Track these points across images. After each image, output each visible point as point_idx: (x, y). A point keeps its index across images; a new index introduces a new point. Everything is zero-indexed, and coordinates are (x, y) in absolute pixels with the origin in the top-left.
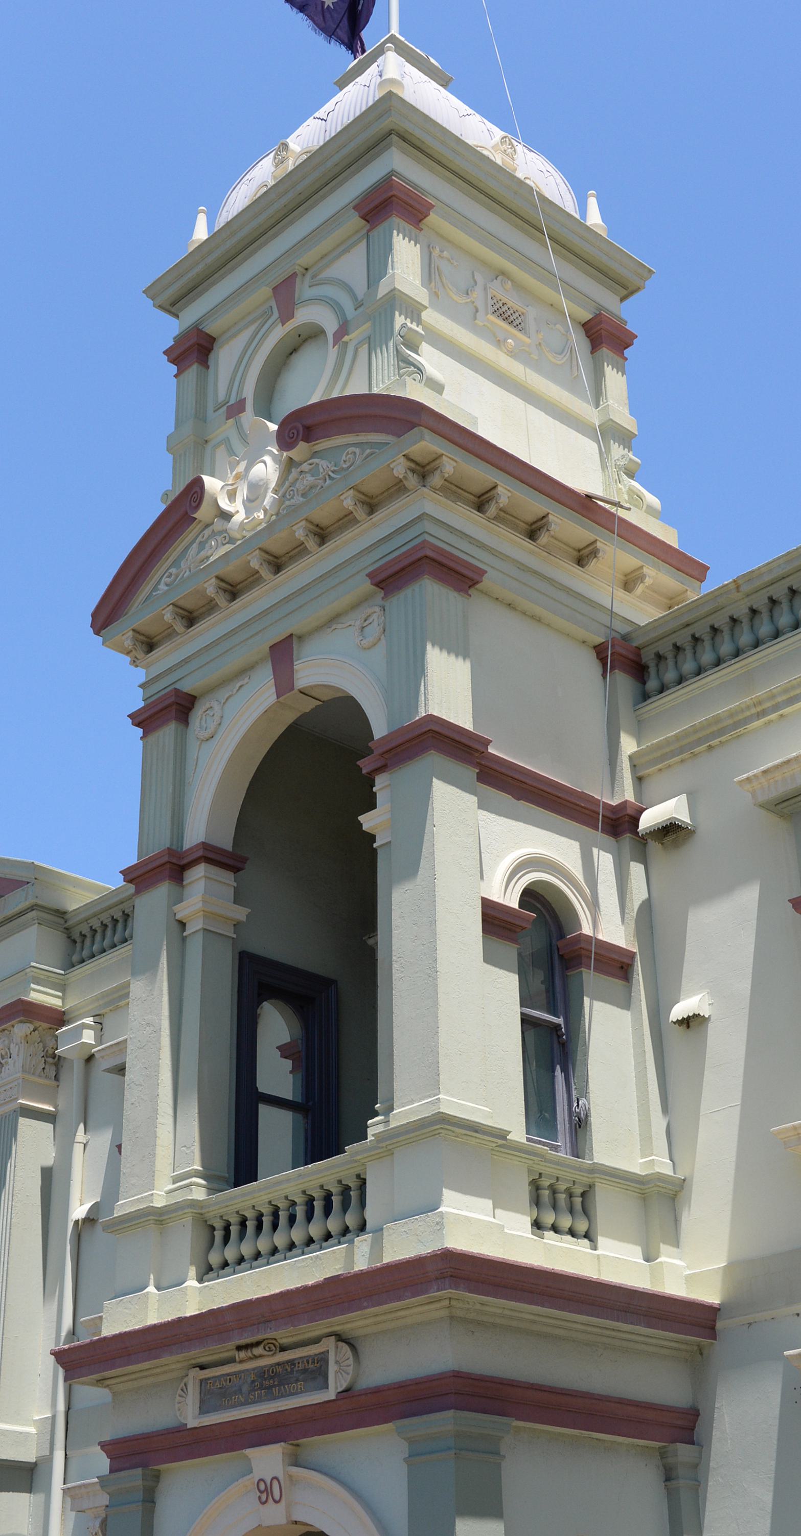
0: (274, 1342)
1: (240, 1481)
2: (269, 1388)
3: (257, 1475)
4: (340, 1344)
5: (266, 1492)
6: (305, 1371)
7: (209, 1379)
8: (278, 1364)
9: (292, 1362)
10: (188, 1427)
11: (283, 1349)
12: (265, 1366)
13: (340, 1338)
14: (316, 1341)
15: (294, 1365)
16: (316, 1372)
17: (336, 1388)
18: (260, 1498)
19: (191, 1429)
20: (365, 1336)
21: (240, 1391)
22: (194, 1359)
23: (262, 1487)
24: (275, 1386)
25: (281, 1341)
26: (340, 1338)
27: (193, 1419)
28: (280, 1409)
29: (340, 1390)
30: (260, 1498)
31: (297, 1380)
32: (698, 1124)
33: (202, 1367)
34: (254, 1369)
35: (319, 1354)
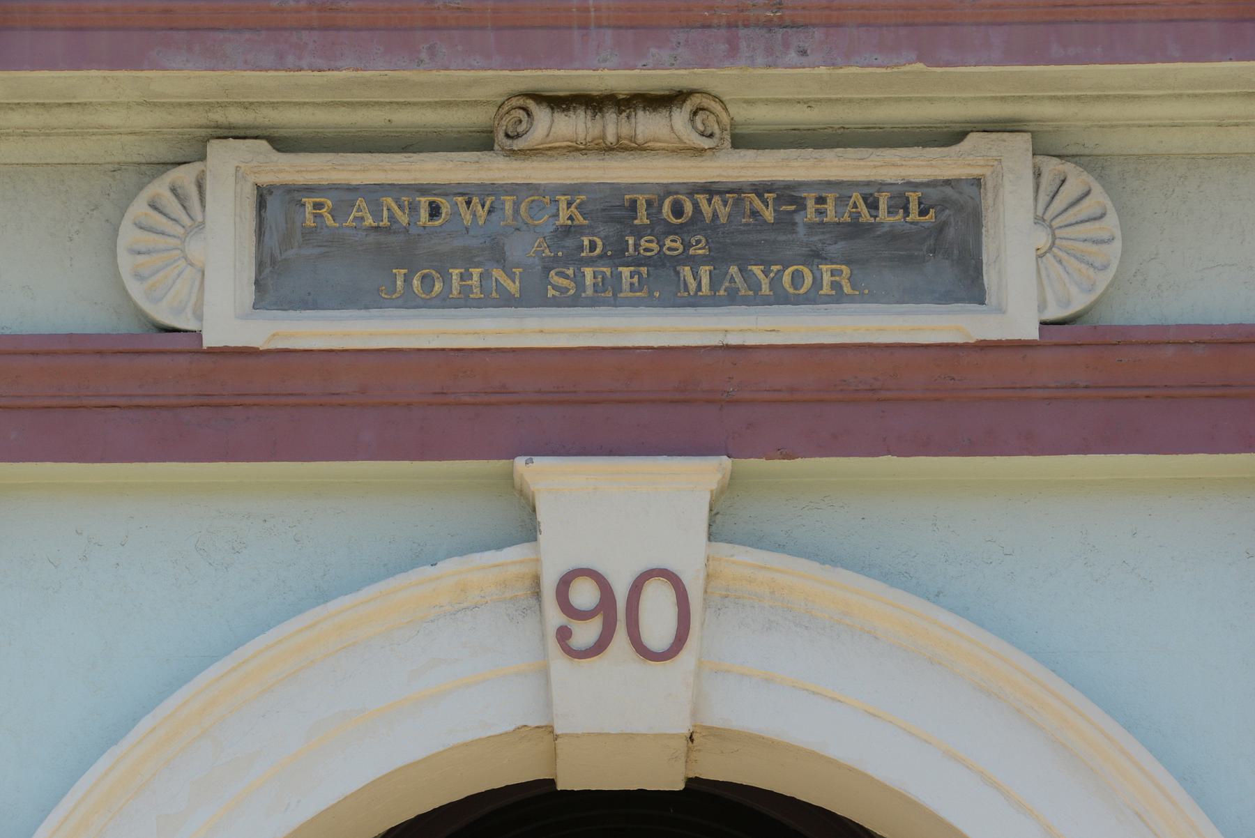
0: (717, 107)
1: (448, 566)
2: (661, 262)
3: (556, 552)
4: (1052, 167)
5: (599, 616)
6: (854, 229)
7: (309, 189)
8: (710, 190)
9: (788, 195)
10: (209, 341)
11: (741, 141)
12: (632, 188)
13: (1046, 144)
14: (952, 136)
15: (800, 204)
16: (937, 241)
17: (1042, 306)
18: (564, 634)
19: (212, 352)
20: (1151, 157)
21: (496, 254)
22: (246, 106)
23: (584, 595)
24: (695, 262)
25: (741, 113)
26: (1046, 144)
27: (225, 310)
28: (733, 340)
29: (1053, 313)
30: (564, 634)
31: (815, 257)
32: (473, 150)
33: (283, 143)
34: (572, 190)
35: (947, 182)
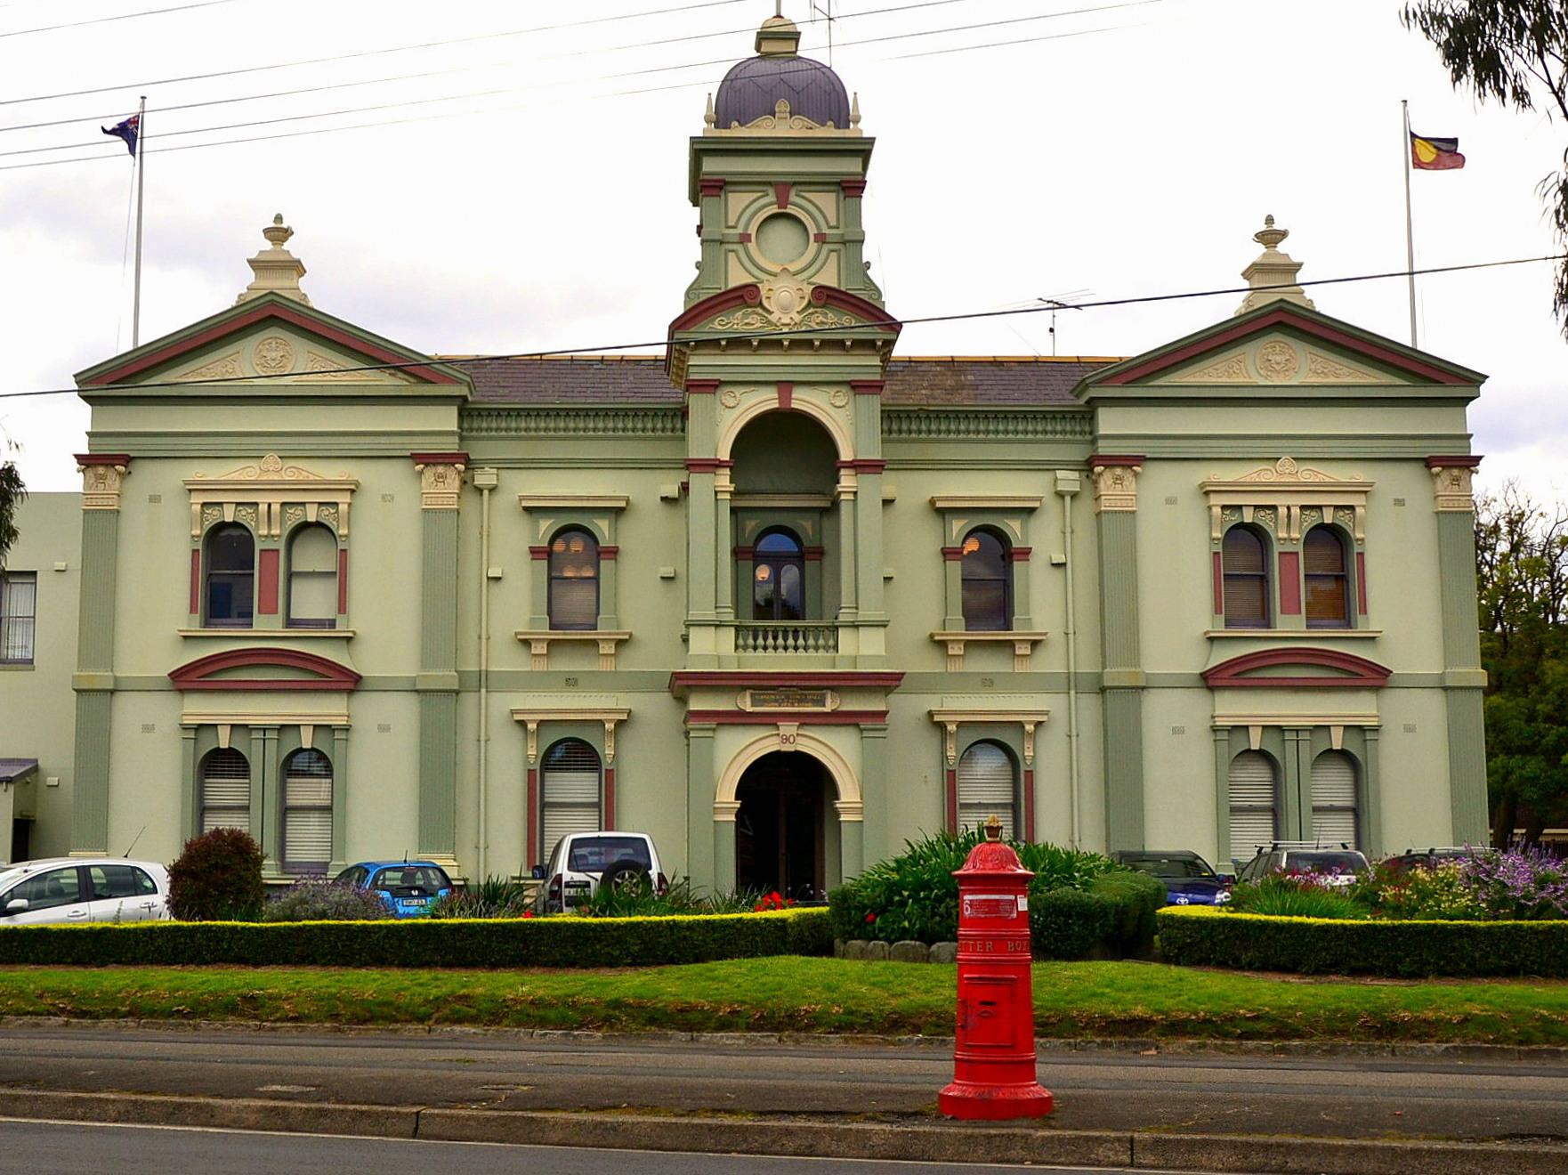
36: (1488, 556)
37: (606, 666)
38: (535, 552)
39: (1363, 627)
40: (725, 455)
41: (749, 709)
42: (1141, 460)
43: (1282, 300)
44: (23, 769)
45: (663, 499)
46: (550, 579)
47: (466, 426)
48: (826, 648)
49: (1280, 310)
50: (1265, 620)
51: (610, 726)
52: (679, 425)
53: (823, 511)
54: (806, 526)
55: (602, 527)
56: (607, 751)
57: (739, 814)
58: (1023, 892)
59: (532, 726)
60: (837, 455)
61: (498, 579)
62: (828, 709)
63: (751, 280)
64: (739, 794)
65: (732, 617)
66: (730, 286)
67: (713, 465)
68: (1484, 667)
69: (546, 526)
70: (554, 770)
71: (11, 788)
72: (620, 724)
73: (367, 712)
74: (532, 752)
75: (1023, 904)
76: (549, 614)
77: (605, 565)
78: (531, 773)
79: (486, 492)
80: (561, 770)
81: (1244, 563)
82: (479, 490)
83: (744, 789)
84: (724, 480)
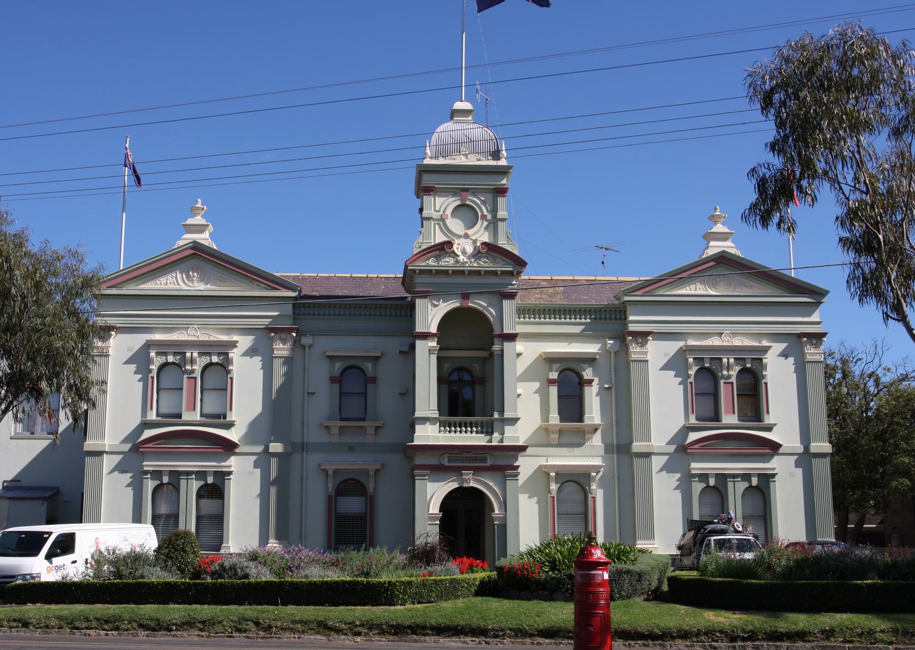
16: (485, 460)
36: (831, 381)
37: (370, 439)
38: (333, 380)
39: (769, 420)
40: (433, 329)
41: (446, 464)
42: (647, 334)
43: (723, 251)
44: (51, 493)
45: (400, 352)
46: (341, 394)
47: (296, 312)
48: (621, 319)
49: (722, 256)
50: (717, 418)
51: (372, 473)
52: (409, 314)
53: (485, 359)
54: (476, 367)
55: (369, 366)
56: (371, 486)
57: (441, 520)
58: (606, 570)
59: (331, 473)
60: (493, 331)
61: (313, 394)
62: (488, 464)
63: (446, 239)
64: (442, 509)
65: (437, 416)
66: (437, 242)
67: (425, 336)
68: (830, 442)
69: (338, 366)
70: (341, 495)
71: (46, 504)
72: (377, 471)
73: (776, 464)
74: (330, 485)
75: (606, 576)
76: (340, 412)
77: (369, 386)
78: (330, 497)
79: (307, 348)
80: (346, 495)
81: (707, 386)
82: (304, 347)
83: (444, 506)
84: (433, 343)
